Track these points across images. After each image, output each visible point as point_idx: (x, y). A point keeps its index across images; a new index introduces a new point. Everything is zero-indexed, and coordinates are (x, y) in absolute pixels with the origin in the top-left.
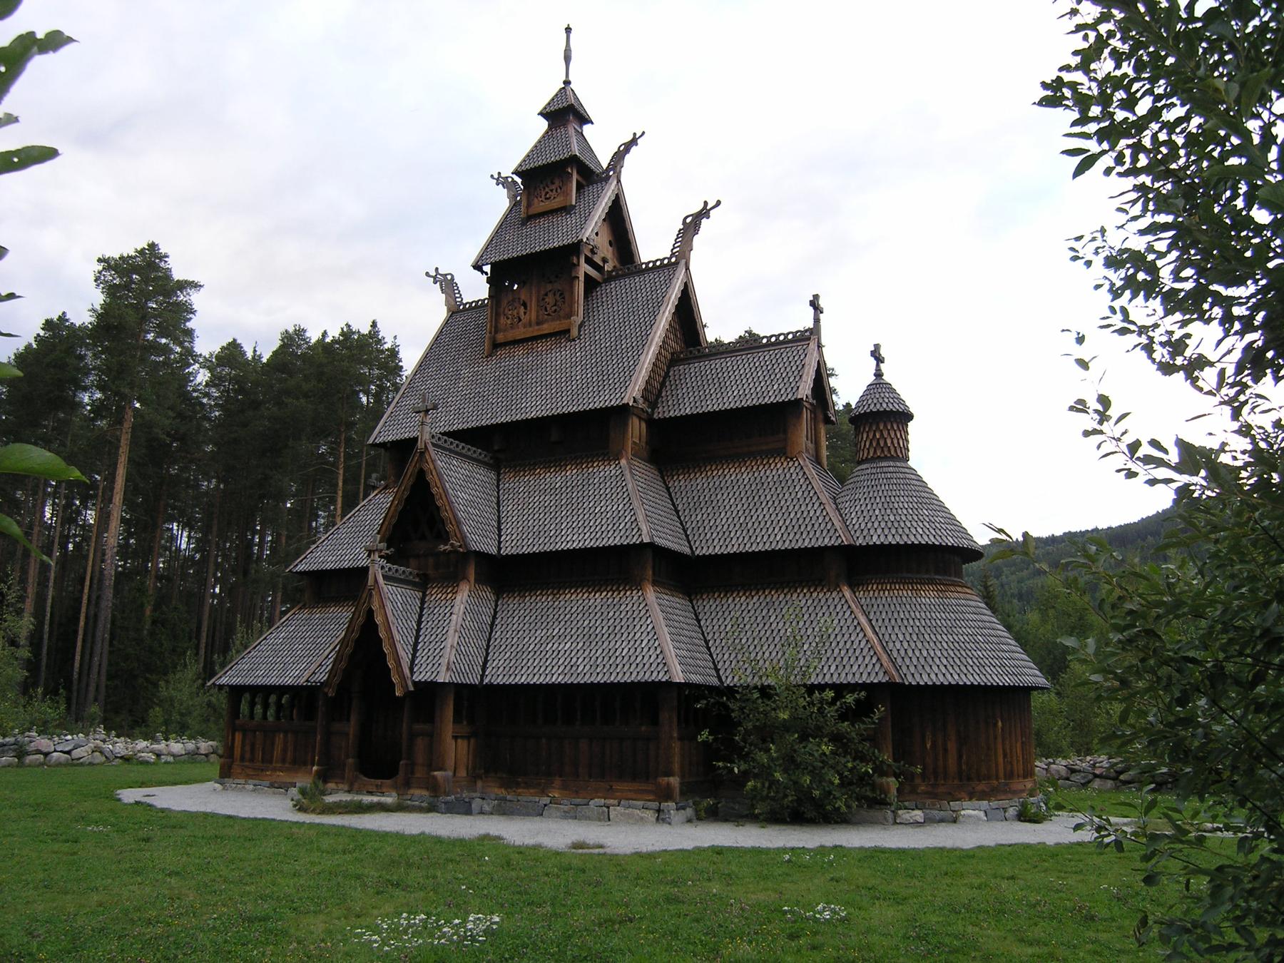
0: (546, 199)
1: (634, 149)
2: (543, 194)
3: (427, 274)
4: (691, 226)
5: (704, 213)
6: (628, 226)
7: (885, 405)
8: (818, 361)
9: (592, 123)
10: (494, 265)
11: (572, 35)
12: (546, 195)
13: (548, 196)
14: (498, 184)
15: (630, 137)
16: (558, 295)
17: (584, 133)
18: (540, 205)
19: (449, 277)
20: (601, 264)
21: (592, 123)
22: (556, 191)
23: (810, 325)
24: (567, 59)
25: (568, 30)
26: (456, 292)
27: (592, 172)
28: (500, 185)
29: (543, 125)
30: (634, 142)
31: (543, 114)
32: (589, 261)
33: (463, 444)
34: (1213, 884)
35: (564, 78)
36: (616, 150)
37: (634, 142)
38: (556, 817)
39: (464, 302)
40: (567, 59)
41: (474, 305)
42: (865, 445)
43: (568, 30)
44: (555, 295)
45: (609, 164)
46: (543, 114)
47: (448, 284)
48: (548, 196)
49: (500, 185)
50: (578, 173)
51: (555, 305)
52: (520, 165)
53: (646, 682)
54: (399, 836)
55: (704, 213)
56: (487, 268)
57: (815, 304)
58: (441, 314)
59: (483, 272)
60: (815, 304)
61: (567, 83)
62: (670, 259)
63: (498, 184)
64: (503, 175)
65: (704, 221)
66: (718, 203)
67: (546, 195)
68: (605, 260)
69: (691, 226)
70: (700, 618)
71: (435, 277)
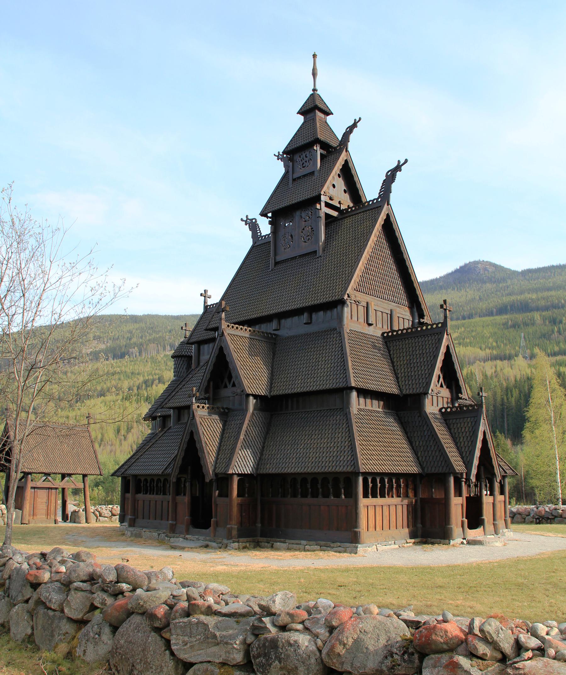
0: (303, 167)
1: (355, 129)
2: (301, 163)
3: (242, 220)
4: (391, 177)
5: (398, 168)
7: (186, 353)
9: (332, 114)
10: (273, 213)
12: (303, 165)
13: (304, 165)
14: (278, 159)
15: (353, 122)
17: (328, 121)
18: (300, 172)
19: (254, 221)
20: (338, 206)
21: (332, 114)
24: (314, 74)
25: (314, 56)
26: (258, 229)
27: (331, 147)
29: (301, 119)
30: (355, 125)
31: (301, 112)
32: (328, 205)
33: (241, 327)
35: (313, 88)
37: (355, 125)
38: (150, 538)
39: (262, 235)
40: (314, 74)
41: (375, 201)
43: (314, 56)
46: (301, 112)
47: (253, 226)
48: (304, 165)
50: (321, 148)
52: (287, 147)
54: (452, 568)
55: (398, 168)
56: (270, 215)
58: (249, 243)
59: (268, 217)
61: (314, 90)
62: (377, 199)
63: (278, 159)
65: (398, 173)
66: (406, 161)
67: (303, 165)
69: (391, 177)
70: (451, 427)
71: (246, 221)
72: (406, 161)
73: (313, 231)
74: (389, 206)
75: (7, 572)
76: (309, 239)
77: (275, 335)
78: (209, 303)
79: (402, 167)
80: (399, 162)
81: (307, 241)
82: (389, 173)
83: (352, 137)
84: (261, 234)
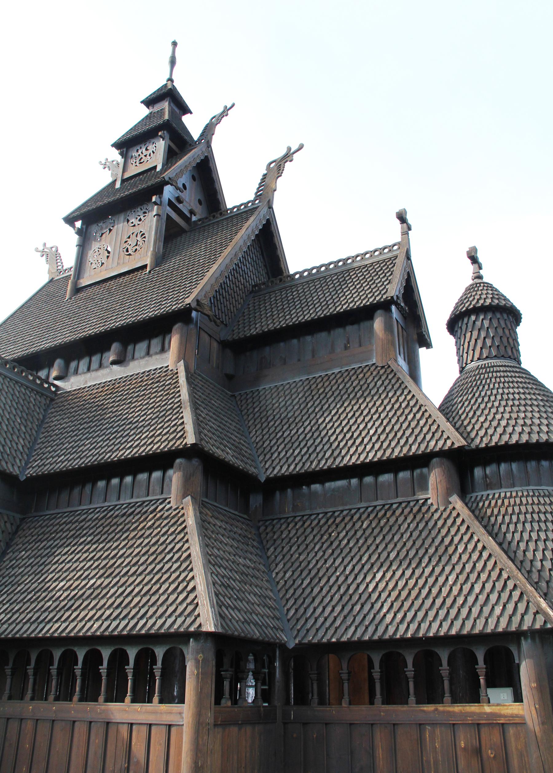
3: (37, 250)
5: (288, 157)
6: (219, 197)
8: (408, 272)
9: (191, 113)
11: (177, 49)
12: (140, 160)
13: (142, 161)
16: (139, 235)
19: (54, 249)
20: (189, 215)
21: (191, 113)
22: (150, 155)
23: (398, 238)
24: (173, 62)
25: (175, 44)
28: (107, 169)
34: (182, 469)
35: (168, 76)
36: (208, 122)
37: (225, 112)
39: (64, 268)
40: (173, 62)
42: (314, 547)
43: (175, 44)
44: (137, 236)
45: (201, 136)
48: (142, 161)
49: (107, 169)
51: (136, 245)
53: (397, 458)
55: (288, 157)
57: (402, 218)
60: (402, 218)
61: (171, 80)
62: (253, 202)
64: (109, 160)
65: (288, 164)
66: (301, 147)
67: (140, 160)
68: (192, 212)
72: (301, 147)
73: (145, 237)
74: (271, 210)
75: (436, 762)
76: (136, 250)
77: (55, 386)
78: (18, 516)
79: (294, 155)
80: (289, 149)
81: (132, 253)
82: (272, 165)
83: (218, 128)
84: (63, 267)
